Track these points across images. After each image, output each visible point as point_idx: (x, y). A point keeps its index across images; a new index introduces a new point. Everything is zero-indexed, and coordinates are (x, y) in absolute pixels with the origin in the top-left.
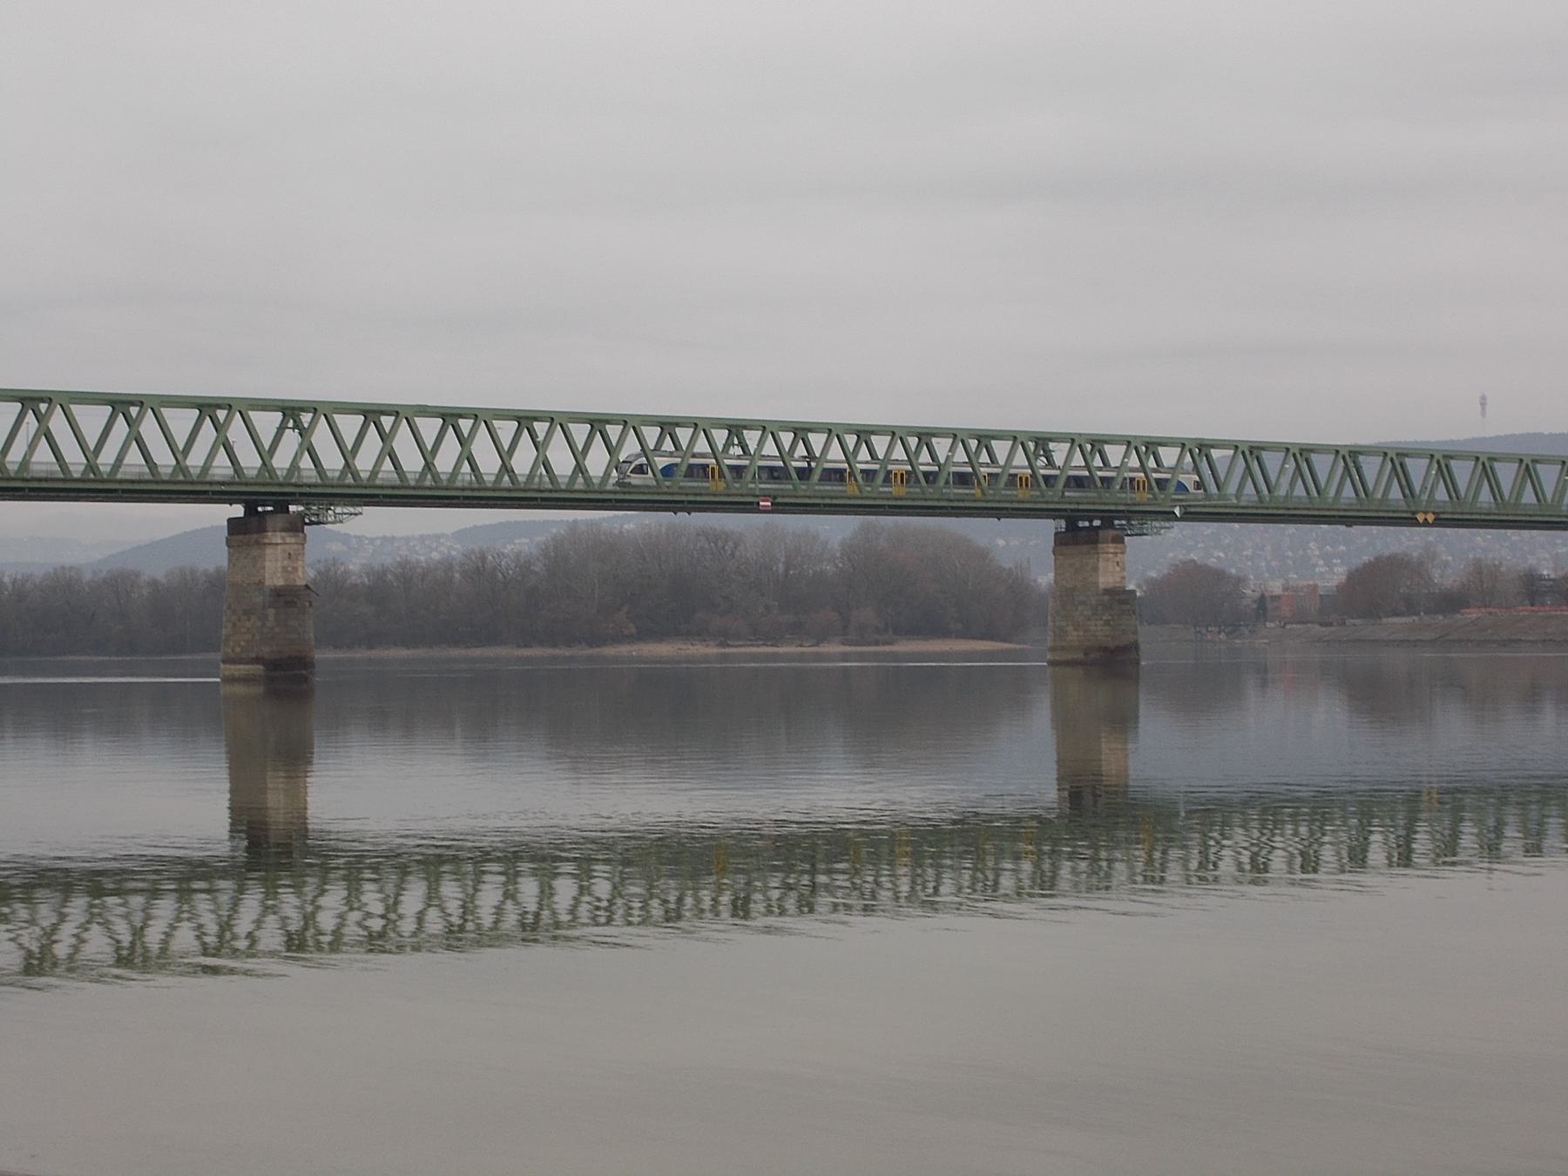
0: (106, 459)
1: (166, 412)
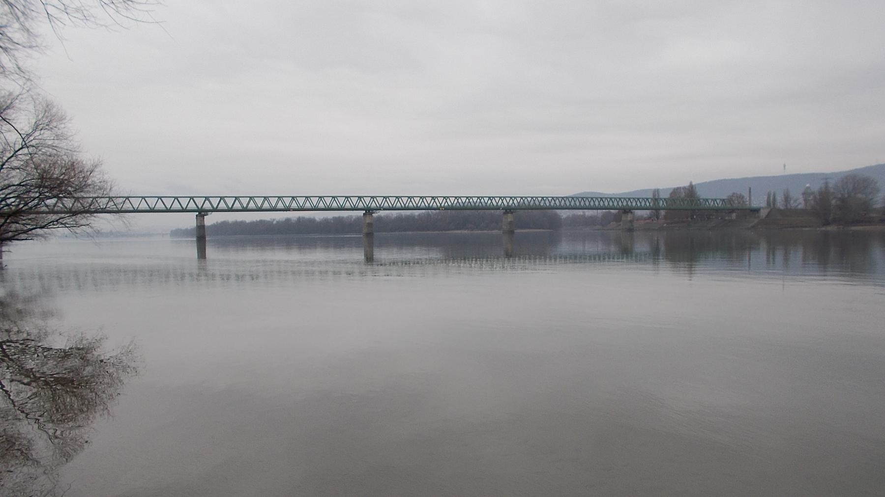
0: (431, 205)
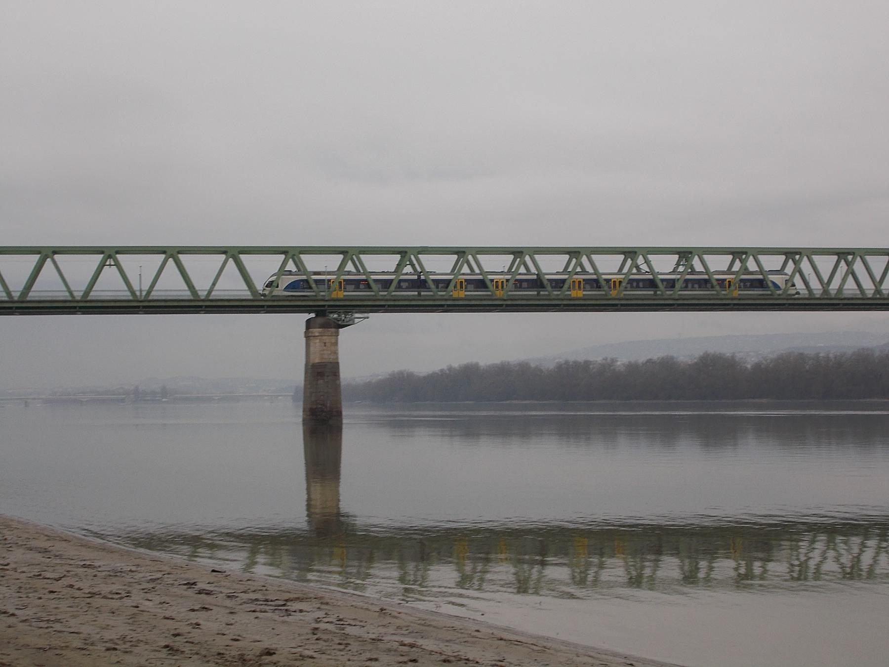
1: (869, 258)
